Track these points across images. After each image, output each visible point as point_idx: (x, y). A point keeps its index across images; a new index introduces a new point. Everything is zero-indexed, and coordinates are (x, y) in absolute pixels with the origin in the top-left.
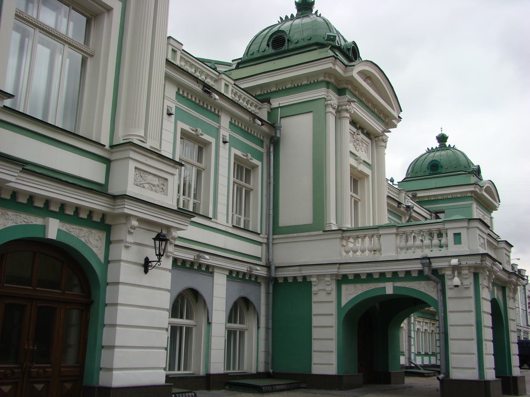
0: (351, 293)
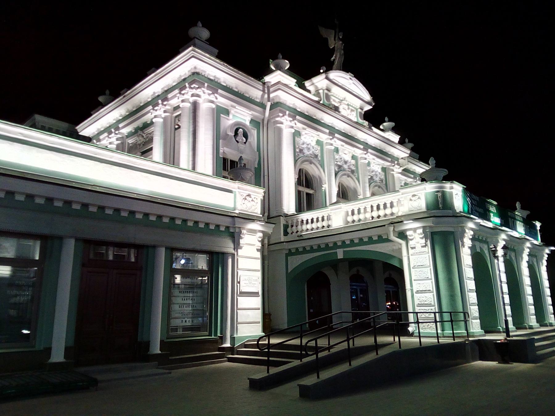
0: (296, 261)
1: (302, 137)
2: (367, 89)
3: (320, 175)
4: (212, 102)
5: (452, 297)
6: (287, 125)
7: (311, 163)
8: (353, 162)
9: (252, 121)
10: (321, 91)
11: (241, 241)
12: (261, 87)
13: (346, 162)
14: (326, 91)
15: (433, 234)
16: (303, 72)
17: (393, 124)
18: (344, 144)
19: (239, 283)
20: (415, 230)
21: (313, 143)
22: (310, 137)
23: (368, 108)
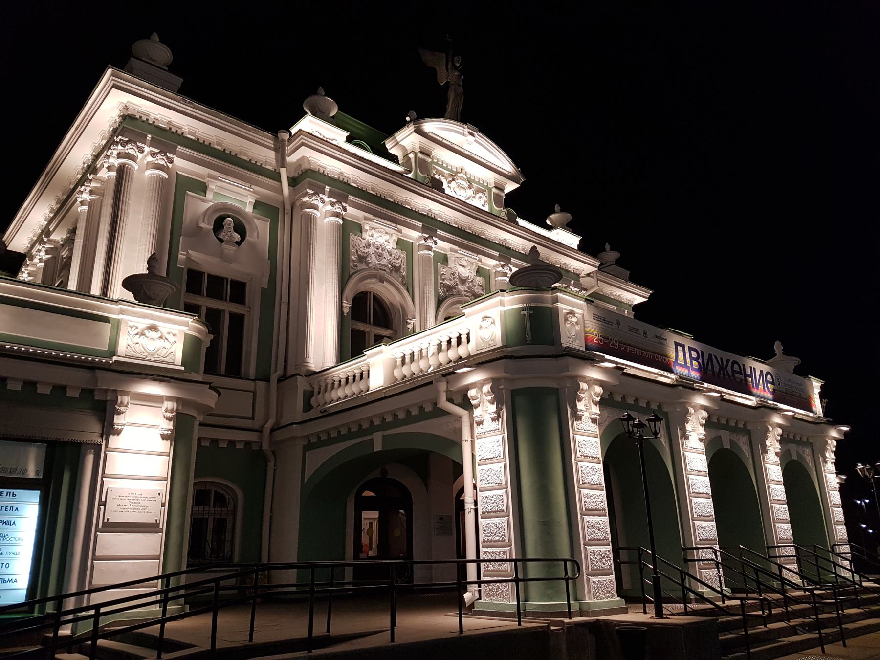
0: (318, 458)
1: (366, 235)
2: (506, 152)
3: (403, 303)
4: (338, 215)
5: (547, 525)
6: (324, 212)
7: (382, 280)
8: (479, 280)
9: (257, 205)
10: (411, 156)
11: (118, 419)
12: (271, 143)
13: (463, 281)
14: (420, 155)
15: (514, 393)
16: (373, 124)
17: (568, 216)
18: (456, 248)
19: (104, 504)
20: (479, 385)
21: (390, 246)
22: (380, 236)
23: (511, 187)
